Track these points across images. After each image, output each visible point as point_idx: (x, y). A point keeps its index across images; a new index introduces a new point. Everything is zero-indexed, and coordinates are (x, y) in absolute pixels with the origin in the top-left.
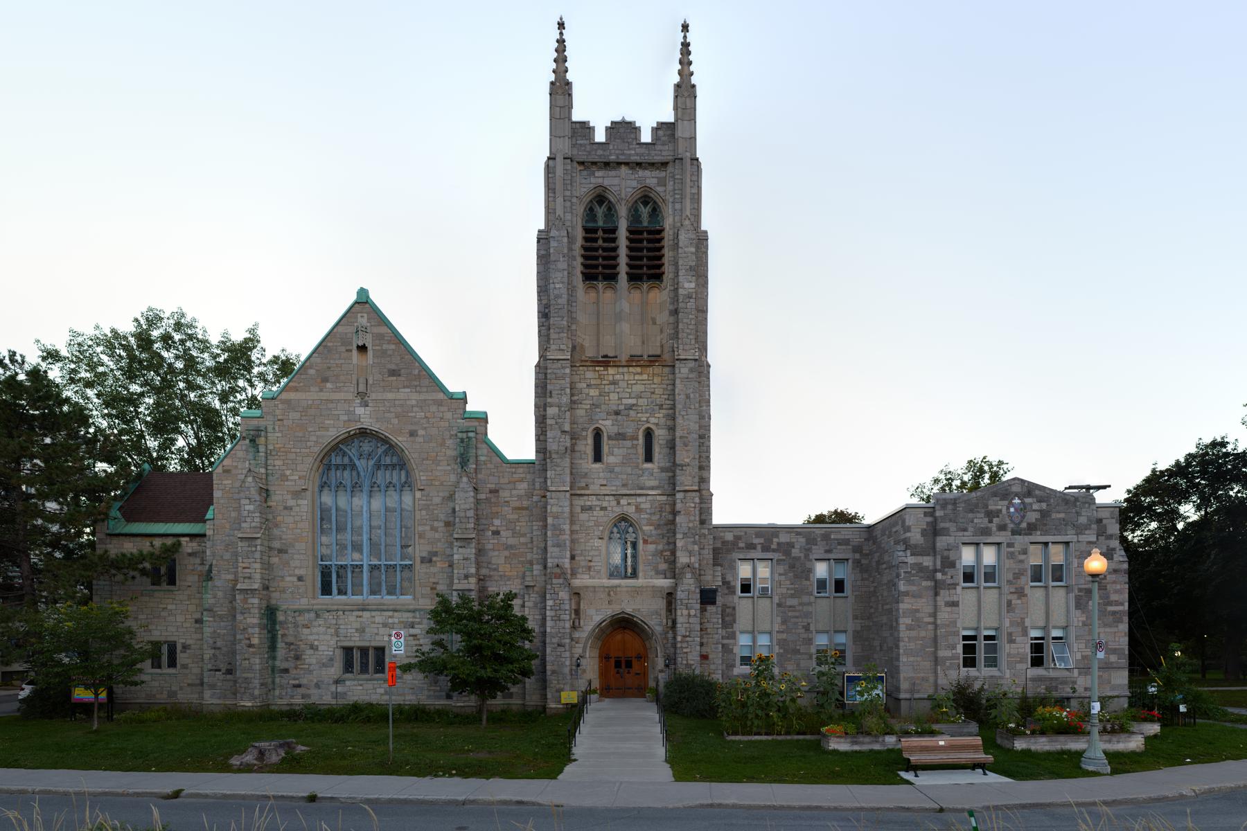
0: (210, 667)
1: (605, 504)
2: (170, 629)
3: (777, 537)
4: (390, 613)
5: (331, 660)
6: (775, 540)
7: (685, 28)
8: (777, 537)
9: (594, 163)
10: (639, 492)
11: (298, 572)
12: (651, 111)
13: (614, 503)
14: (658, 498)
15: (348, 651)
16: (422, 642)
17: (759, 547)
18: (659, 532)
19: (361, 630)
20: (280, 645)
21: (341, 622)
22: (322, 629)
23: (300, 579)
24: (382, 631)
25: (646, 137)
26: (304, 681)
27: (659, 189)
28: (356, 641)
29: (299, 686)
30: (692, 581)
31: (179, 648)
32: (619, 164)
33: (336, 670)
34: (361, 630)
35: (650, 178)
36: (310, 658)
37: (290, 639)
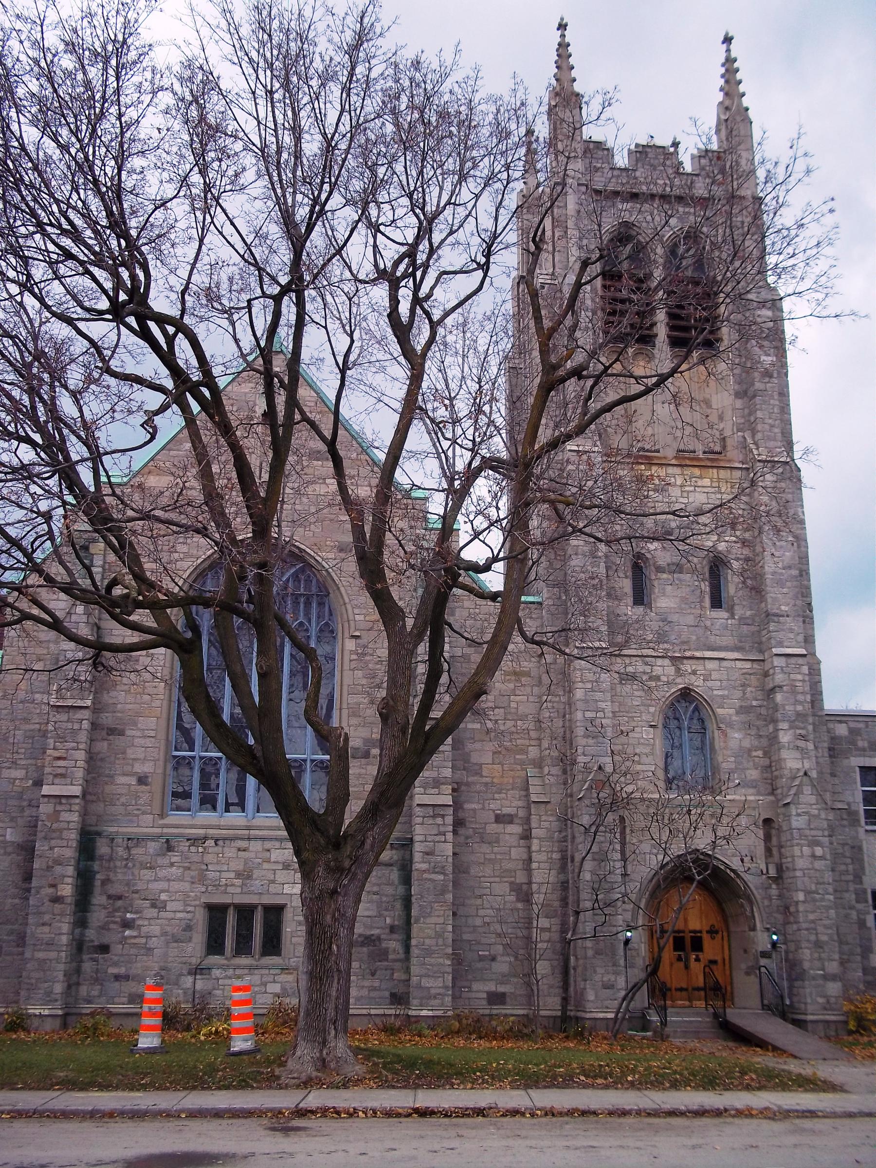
1: (658, 671)
5: (189, 928)
7: (562, 27)
9: (616, 193)
10: (708, 654)
11: (139, 768)
12: (691, 130)
13: (671, 670)
14: (739, 664)
19: (245, 875)
20: (98, 899)
21: (209, 858)
23: (142, 780)
28: (236, 895)
29: (127, 978)
30: (813, 799)
34: (245, 875)
36: (152, 926)
37: (116, 889)
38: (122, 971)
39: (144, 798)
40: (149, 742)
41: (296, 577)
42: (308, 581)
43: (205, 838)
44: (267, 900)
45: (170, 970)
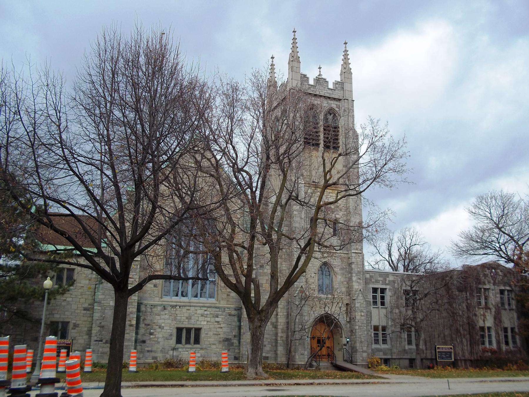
0: (95, 338)
2: (67, 313)
3: (388, 277)
4: (206, 309)
6: (388, 279)
8: (388, 277)
15: (179, 330)
16: (222, 325)
17: (381, 282)
18: (342, 271)
19: (189, 318)
20: (142, 325)
22: (167, 316)
24: (201, 319)
25: (331, 86)
26: (154, 349)
27: (337, 109)
29: (151, 351)
30: (362, 298)
31: (71, 326)
32: (321, 96)
33: (173, 341)
34: (189, 318)
35: (333, 104)
37: (147, 322)
39: (156, 292)
43: (176, 306)
44: (196, 326)
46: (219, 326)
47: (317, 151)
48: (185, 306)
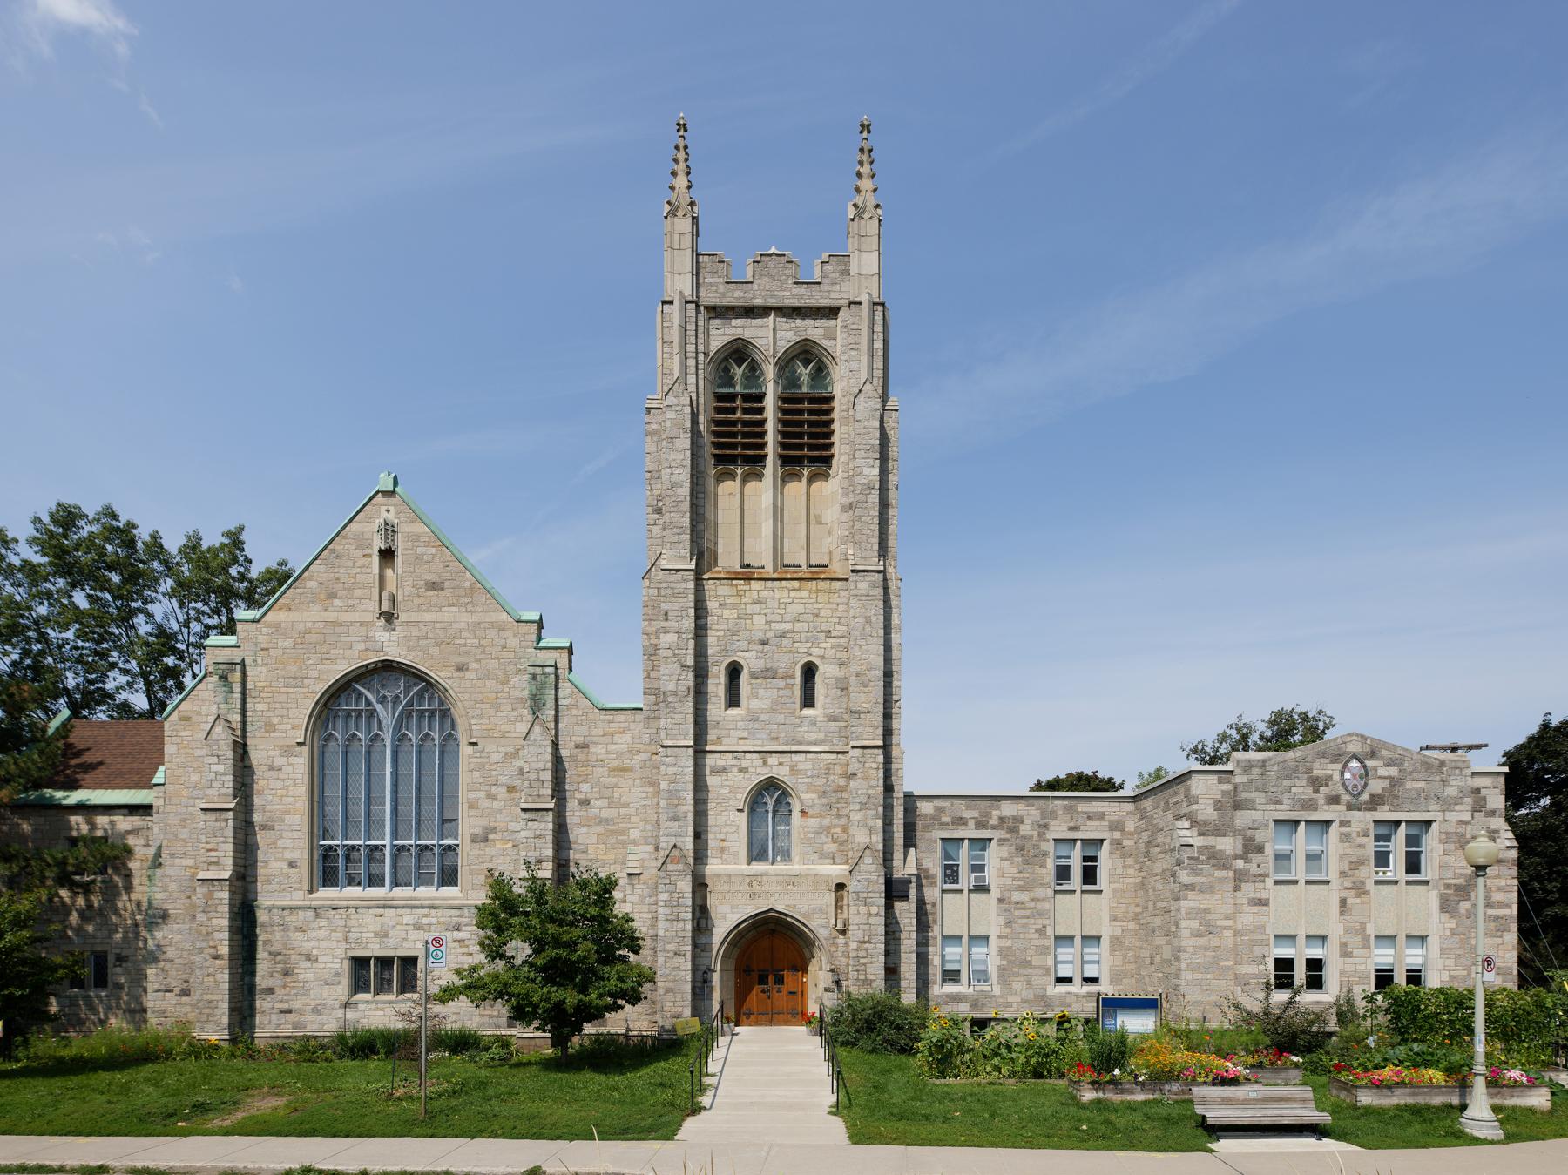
0: (157, 986)
11: (289, 855)
15: (360, 963)
23: (292, 865)
26: (296, 1005)
28: (374, 949)
29: (289, 1011)
31: (111, 960)
33: (343, 989)
35: (813, 329)
38: (285, 1006)
39: (294, 878)
40: (295, 834)
41: (420, 695)
42: (431, 698)
43: (347, 907)
44: (401, 953)
45: (1093, 1083)
46: (464, 950)
47: (760, 476)
48: (369, 907)
